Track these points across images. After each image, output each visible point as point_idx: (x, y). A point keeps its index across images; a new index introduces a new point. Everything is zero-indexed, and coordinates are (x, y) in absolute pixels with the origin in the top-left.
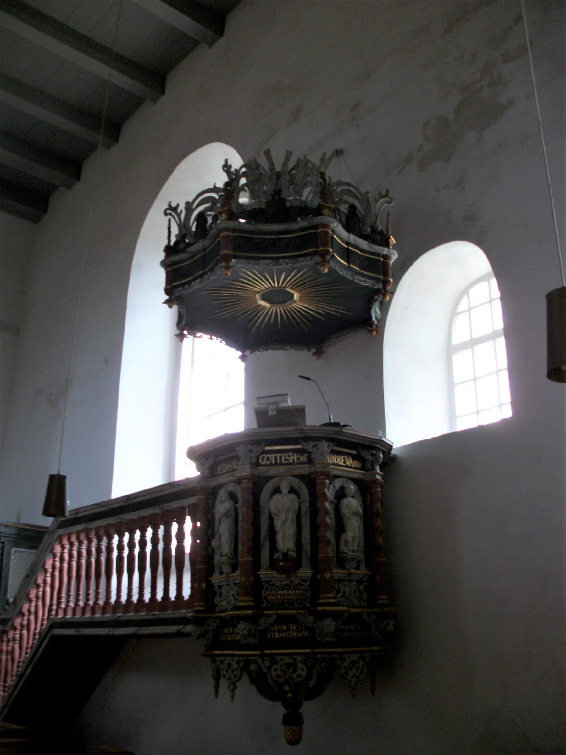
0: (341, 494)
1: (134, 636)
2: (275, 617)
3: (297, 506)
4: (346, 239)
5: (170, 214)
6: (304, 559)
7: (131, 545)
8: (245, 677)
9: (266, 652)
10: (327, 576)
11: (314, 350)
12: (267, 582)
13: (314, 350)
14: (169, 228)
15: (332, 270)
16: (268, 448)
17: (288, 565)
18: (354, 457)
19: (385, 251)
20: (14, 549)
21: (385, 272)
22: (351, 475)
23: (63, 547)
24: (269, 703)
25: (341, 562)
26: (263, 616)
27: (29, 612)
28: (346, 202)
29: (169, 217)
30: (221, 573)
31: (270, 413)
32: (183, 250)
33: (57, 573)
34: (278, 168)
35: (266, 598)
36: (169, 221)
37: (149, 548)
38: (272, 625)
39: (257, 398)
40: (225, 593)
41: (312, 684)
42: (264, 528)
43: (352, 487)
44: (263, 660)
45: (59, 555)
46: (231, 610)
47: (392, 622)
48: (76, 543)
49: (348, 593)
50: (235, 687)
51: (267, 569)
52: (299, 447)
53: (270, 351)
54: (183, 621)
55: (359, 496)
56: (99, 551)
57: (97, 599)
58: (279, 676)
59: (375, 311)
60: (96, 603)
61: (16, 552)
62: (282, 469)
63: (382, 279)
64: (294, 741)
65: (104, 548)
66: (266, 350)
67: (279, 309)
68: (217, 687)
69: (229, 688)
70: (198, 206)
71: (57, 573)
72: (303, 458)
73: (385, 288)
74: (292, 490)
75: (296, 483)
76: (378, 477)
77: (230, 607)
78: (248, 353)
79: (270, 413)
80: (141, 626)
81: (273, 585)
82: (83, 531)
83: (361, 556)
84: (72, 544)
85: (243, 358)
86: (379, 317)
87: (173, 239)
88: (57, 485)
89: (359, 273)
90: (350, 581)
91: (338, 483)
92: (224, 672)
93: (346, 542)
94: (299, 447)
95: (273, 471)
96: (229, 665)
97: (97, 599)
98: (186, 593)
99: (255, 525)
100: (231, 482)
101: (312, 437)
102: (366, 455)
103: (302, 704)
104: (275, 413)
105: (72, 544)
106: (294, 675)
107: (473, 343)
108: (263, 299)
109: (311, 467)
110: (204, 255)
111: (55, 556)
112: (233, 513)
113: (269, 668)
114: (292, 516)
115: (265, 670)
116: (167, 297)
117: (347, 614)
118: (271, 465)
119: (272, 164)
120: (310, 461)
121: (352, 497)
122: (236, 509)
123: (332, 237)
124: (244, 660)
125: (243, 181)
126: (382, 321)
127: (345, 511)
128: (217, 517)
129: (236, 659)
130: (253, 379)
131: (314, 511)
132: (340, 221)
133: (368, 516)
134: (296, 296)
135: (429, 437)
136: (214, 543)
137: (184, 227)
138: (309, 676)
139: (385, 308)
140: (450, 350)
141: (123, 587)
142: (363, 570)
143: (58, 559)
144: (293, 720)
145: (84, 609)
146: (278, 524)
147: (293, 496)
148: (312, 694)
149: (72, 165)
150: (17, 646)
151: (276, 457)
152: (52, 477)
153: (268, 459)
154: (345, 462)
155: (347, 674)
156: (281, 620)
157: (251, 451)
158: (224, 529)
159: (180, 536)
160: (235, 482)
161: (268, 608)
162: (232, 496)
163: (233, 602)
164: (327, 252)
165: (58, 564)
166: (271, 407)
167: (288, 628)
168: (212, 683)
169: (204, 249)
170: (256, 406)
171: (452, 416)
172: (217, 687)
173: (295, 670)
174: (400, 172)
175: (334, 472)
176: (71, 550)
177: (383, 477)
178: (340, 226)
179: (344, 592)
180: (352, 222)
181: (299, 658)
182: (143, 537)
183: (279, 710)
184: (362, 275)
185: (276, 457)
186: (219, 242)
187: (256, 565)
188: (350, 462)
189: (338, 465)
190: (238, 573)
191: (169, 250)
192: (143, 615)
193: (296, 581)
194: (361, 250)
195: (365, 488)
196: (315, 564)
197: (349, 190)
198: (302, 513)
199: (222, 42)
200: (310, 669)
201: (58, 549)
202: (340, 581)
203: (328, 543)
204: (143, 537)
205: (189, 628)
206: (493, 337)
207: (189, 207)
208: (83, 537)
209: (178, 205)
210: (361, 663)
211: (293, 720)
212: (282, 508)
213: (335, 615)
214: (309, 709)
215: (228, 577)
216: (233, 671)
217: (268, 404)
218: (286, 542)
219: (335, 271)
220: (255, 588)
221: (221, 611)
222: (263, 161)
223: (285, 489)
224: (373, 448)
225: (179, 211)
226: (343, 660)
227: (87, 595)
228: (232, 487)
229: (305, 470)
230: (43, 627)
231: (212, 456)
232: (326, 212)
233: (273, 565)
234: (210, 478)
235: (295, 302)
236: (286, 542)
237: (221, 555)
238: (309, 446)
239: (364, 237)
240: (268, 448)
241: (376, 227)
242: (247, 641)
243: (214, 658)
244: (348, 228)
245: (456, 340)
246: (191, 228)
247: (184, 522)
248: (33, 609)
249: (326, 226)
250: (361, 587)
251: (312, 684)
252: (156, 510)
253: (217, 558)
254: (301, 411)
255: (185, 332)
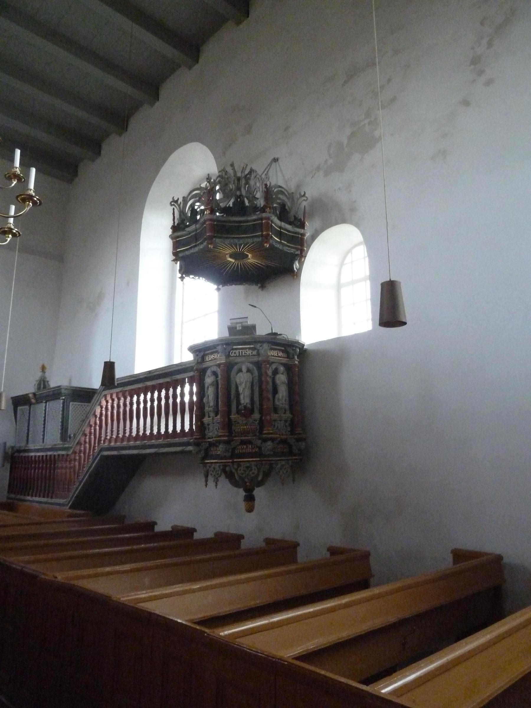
0: (276, 372)
1: (156, 454)
2: (240, 441)
3: (251, 380)
4: (280, 225)
5: (174, 205)
6: (255, 409)
7: (152, 400)
8: (223, 476)
9: (235, 460)
10: (268, 417)
11: (259, 285)
12: (235, 421)
13: (259, 285)
14: (174, 214)
15: (271, 246)
16: (235, 347)
17: (248, 412)
18: (283, 351)
19: (302, 231)
20: (71, 403)
21: (302, 245)
22: (281, 362)
23: (107, 402)
24: (235, 489)
25: (276, 410)
26: (233, 440)
27: (85, 442)
28: (280, 199)
29: (173, 207)
30: (209, 417)
31: (238, 328)
32: (183, 229)
33: (104, 418)
34: (239, 174)
35: (234, 430)
36: (174, 209)
37: (163, 402)
38: (238, 445)
39: (231, 319)
40: (211, 428)
41: (260, 478)
42: (233, 391)
43: (282, 369)
44: (233, 464)
45: (104, 407)
46: (215, 437)
47: (304, 444)
48: (116, 399)
49: (279, 427)
50: (218, 481)
51: (235, 415)
52: (252, 346)
53: (234, 286)
54: (187, 444)
55: (285, 373)
56: (125, 405)
57: (118, 434)
58: (242, 474)
59: (296, 265)
60: (111, 437)
61: (72, 404)
62: (243, 359)
63: (299, 246)
64: (250, 510)
65: (128, 403)
66: (232, 285)
67: (239, 263)
68: (206, 481)
69: (214, 481)
70: (190, 200)
71: (104, 418)
72: (255, 353)
73: (301, 253)
74: (248, 371)
75: (251, 366)
76: (297, 362)
77: (214, 436)
78: (221, 286)
79: (238, 328)
80: (159, 448)
81: (238, 423)
82: (121, 391)
83: (287, 407)
84: (113, 400)
85: (218, 289)
86: (298, 267)
87: (176, 222)
88: (109, 367)
89: (287, 246)
90: (280, 421)
91: (274, 366)
92: (211, 472)
93: (278, 399)
94: (252, 346)
95: (239, 360)
96: (214, 468)
97: (118, 434)
98: (187, 428)
99: (228, 391)
100: (214, 365)
101: (261, 341)
102: (291, 351)
103: (254, 489)
104: (240, 328)
105: (113, 400)
106: (251, 473)
107: (353, 283)
108: (231, 257)
109: (258, 358)
110: (196, 234)
111: (102, 407)
112: (215, 383)
113: (237, 470)
114: (249, 384)
115: (233, 471)
116: (174, 258)
117: (279, 439)
118: (236, 356)
119: (235, 172)
120: (258, 354)
121: (282, 374)
122: (217, 381)
123: (271, 225)
124: (223, 466)
125: (217, 188)
126: (300, 270)
127: (278, 382)
128: (206, 385)
129: (218, 465)
130: (224, 303)
131: (260, 382)
132: (276, 215)
133: (291, 384)
134: (250, 256)
135: (325, 339)
136: (205, 400)
137: (182, 213)
138: (258, 475)
139: (301, 264)
140: (339, 286)
141: (138, 426)
142: (288, 415)
143: (104, 409)
144: (250, 499)
145: (110, 441)
146: (241, 389)
147: (249, 374)
148: (260, 484)
149: (94, 146)
150: (77, 463)
151: (239, 352)
152: (106, 363)
153: (235, 353)
154: (278, 354)
155: (279, 472)
156: (243, 442)
157: (225, 349)
158: (210, 392)
159: (182, 395)
160: (216, 365)
161: (235, 436)
162: (215, 374)
163: (216, 433)
164: (268, 235)
165: (104, 412)
166: (238, 325)
167: (247, 447)
168: (203, 479)
169: (196, 230)
170: (230, 324)
171: (339, 325)
172: (206, 481)
173: (251, 470)
174: (313, 177)
175: (272, 360)
176: (113, 404)
177: (299, 362)
178: (276, 218)
179: (278, 427)
180: (284, 214)
181: (253, 463)
182: (159, 395)
183: (242, 493)
184: (289, 246)
185: (239, 352)
186: (205, 227)
187: (229, 413)
188: (280, 354)
189: (273, 356)
190: (219, 417)
191: (175, 228)
192: (160, 441)
193: (251, 421)
194: (289, 231)
195: (289, 368)
196: (261, 412)
197: (282, 191)
198: (254, 383)
199: (197, 67)
200: (259, 470)
201: (104, 403)
202: (275, 421)
203: (268, 399)
204: (159, 395)
205: (190, 448)
206: (364, 279)
207: (185, 200)
208: (120, 395)
209: (178, 199)
210: (287, 466)
211: (250, 499)
212: (243, 380)
213: (273, 440)
214: (258, 492)
215: (213, 419)
216: (217, 471)
217: (237, 323)
218: (245, 400)
219: (273, 245)
220: (228, 425)
221: (209, 438)
222: (229, 169)
223: (244, 369)
224: (293, 346)
225: (179, 203)
226: (277, 464)
227: (118, 431)
228: (215, 369)
229: (256, 359)
230: (96, 451)
231: (201, 351)
232: (268, 210)
233: (238, 412)
234: (201, 363)
235: (249, 259)
236: (245, 400)
237: (209, 407)
238: (258, 346)
239: (290, 223)
240: (235, 347)
241: (297, 216)
242: (225, 454)
243: (205, 464)
244: (280, 219)
245: (343, 281)
246: (186, 214)
247: (185, 386)
248: (87, 440)
249: (268, 218)
250: (287, 424)
251: (260, 478)
252: (168, 380)
253: (207, 408)
254: (254, 327)
255: (184, 276)
